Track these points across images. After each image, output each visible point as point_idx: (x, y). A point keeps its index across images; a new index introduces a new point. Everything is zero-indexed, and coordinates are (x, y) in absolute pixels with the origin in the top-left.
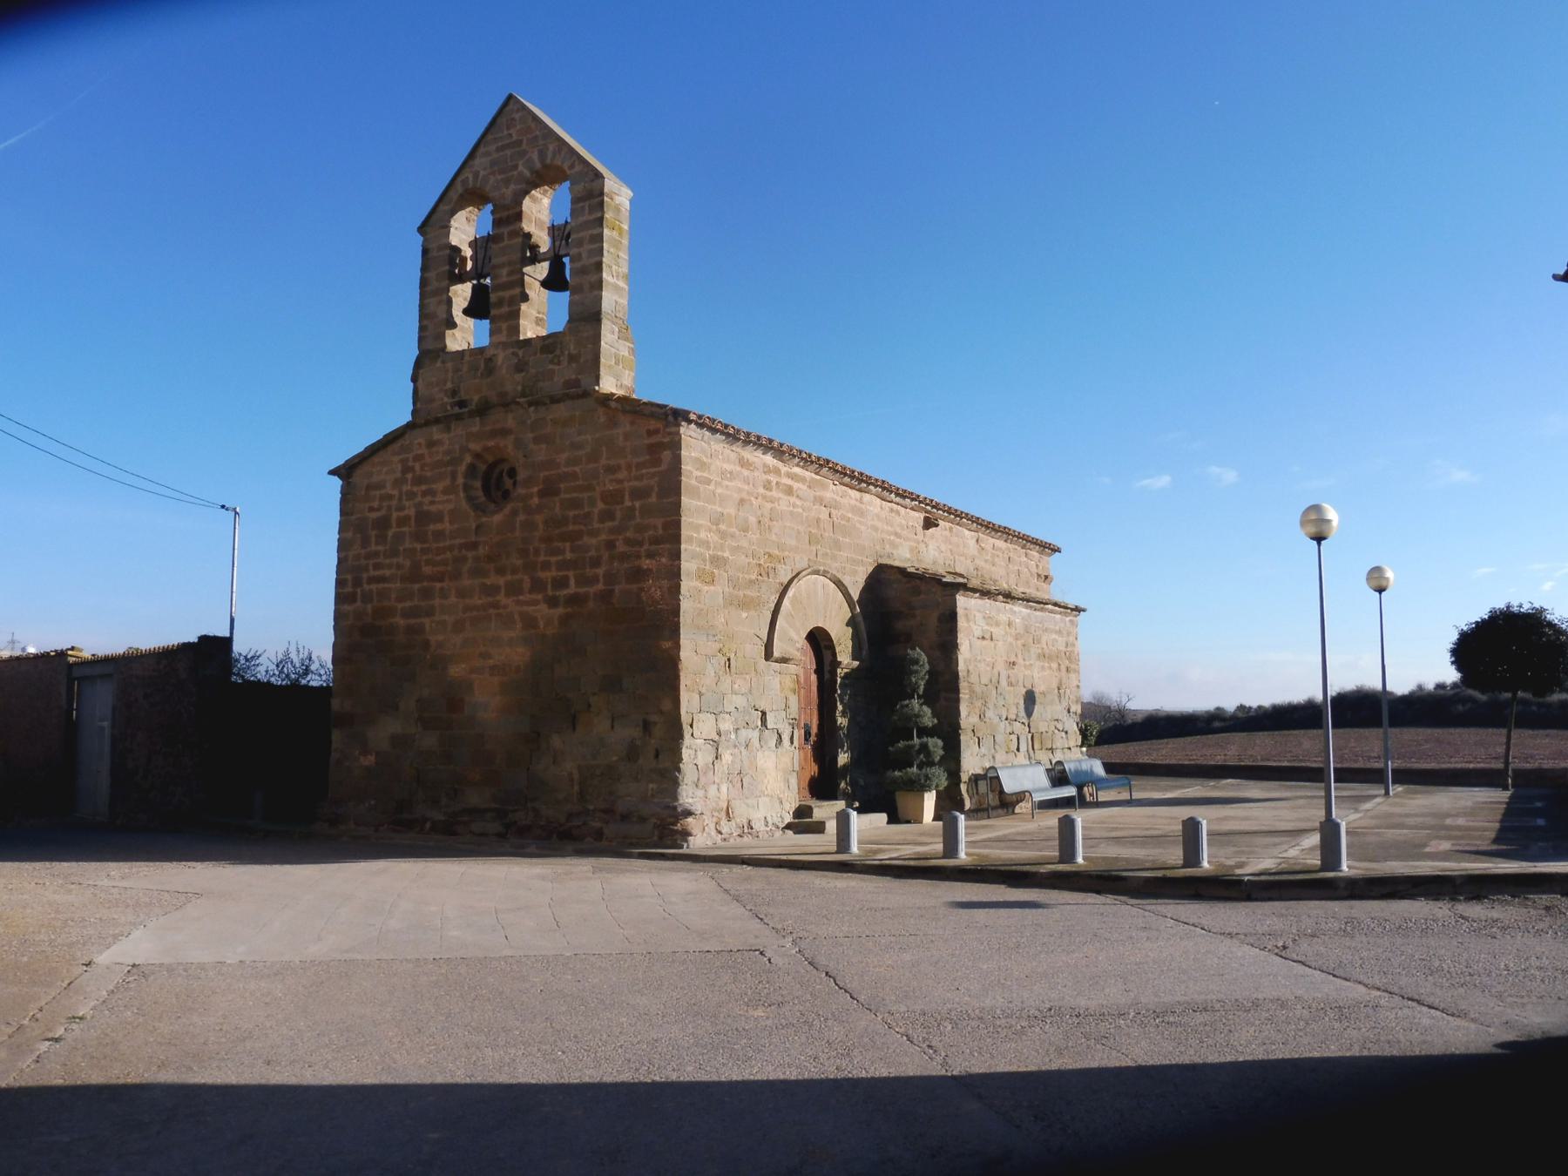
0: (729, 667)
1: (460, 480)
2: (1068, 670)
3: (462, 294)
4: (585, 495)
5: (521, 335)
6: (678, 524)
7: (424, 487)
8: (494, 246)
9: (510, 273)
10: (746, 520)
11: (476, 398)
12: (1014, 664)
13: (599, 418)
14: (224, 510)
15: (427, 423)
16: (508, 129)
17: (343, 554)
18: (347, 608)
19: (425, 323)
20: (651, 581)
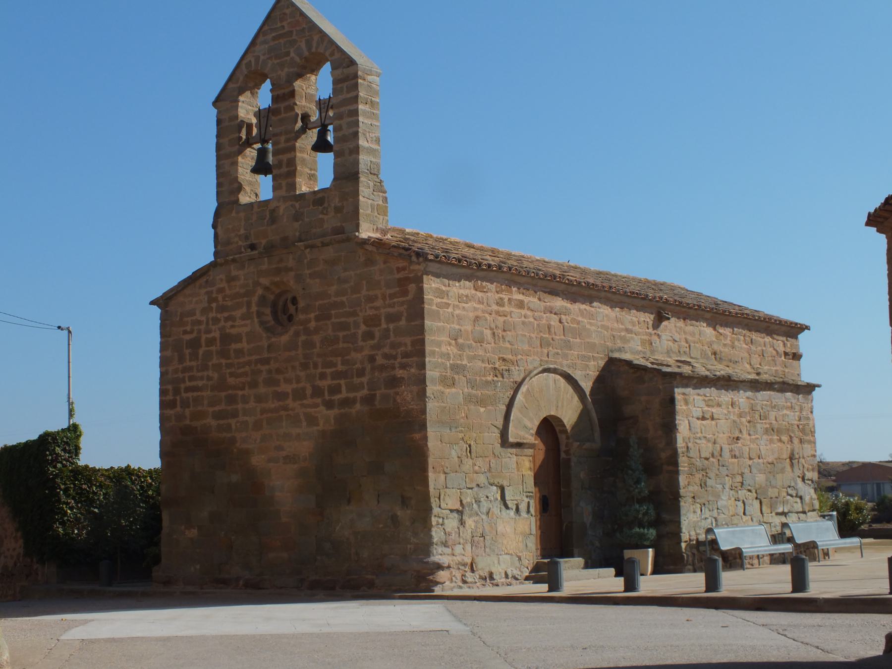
0: (470, 452)
1: (254, 308)
2: (801, 441)
4: (351, 320)
5: (297, 191)
6: (422, 342)
7: (226, 314)
8: (273, 118)
9: (287, 141)
10: (482, 333)
11: (264, 242)
12: (738, 439)
15: (226, 262)
16: (281, 21)
17: (164, 369)
19: (221, 180)
20: (403, 387)
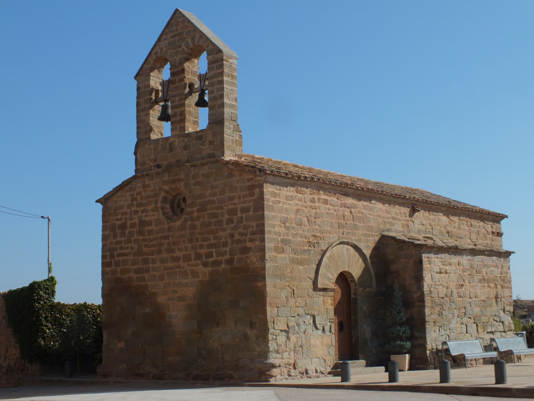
0: (293, 294)
1: (160, 204)
3: (156, 111)
4: (219, 211)
5: (186, 131)
6: (263, 225)
7: (142, 208)
9: (180, 100)
10: (301, 220)
11: (165, 163)
12: (462, 285)
13: (224, 172)
14: (43, 219)
15: (143, 176)
16: (176, 26)
17: (104, 242)
18: (108, 269)
19: (139, 125)
